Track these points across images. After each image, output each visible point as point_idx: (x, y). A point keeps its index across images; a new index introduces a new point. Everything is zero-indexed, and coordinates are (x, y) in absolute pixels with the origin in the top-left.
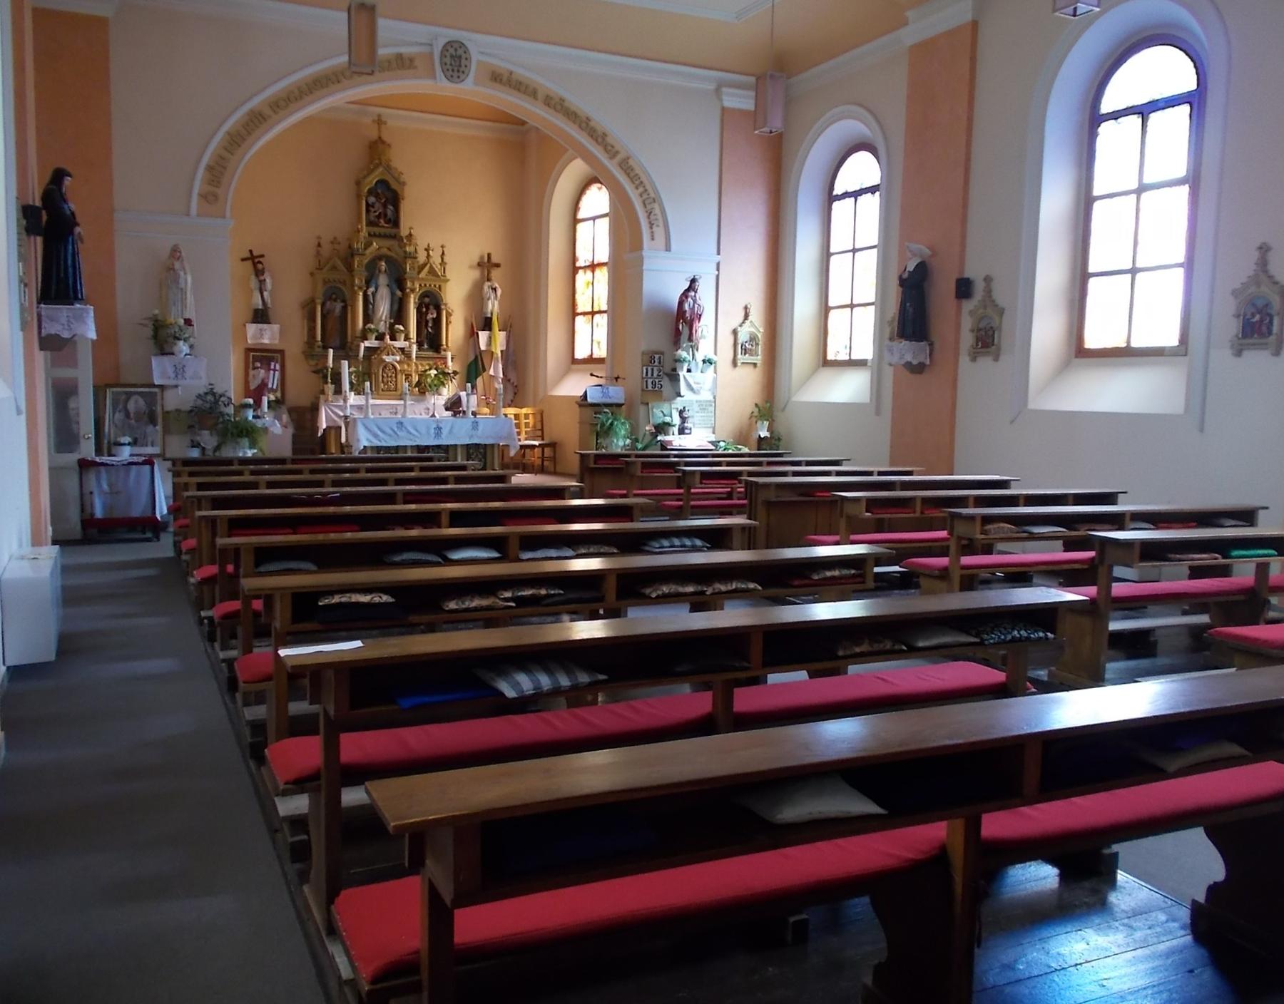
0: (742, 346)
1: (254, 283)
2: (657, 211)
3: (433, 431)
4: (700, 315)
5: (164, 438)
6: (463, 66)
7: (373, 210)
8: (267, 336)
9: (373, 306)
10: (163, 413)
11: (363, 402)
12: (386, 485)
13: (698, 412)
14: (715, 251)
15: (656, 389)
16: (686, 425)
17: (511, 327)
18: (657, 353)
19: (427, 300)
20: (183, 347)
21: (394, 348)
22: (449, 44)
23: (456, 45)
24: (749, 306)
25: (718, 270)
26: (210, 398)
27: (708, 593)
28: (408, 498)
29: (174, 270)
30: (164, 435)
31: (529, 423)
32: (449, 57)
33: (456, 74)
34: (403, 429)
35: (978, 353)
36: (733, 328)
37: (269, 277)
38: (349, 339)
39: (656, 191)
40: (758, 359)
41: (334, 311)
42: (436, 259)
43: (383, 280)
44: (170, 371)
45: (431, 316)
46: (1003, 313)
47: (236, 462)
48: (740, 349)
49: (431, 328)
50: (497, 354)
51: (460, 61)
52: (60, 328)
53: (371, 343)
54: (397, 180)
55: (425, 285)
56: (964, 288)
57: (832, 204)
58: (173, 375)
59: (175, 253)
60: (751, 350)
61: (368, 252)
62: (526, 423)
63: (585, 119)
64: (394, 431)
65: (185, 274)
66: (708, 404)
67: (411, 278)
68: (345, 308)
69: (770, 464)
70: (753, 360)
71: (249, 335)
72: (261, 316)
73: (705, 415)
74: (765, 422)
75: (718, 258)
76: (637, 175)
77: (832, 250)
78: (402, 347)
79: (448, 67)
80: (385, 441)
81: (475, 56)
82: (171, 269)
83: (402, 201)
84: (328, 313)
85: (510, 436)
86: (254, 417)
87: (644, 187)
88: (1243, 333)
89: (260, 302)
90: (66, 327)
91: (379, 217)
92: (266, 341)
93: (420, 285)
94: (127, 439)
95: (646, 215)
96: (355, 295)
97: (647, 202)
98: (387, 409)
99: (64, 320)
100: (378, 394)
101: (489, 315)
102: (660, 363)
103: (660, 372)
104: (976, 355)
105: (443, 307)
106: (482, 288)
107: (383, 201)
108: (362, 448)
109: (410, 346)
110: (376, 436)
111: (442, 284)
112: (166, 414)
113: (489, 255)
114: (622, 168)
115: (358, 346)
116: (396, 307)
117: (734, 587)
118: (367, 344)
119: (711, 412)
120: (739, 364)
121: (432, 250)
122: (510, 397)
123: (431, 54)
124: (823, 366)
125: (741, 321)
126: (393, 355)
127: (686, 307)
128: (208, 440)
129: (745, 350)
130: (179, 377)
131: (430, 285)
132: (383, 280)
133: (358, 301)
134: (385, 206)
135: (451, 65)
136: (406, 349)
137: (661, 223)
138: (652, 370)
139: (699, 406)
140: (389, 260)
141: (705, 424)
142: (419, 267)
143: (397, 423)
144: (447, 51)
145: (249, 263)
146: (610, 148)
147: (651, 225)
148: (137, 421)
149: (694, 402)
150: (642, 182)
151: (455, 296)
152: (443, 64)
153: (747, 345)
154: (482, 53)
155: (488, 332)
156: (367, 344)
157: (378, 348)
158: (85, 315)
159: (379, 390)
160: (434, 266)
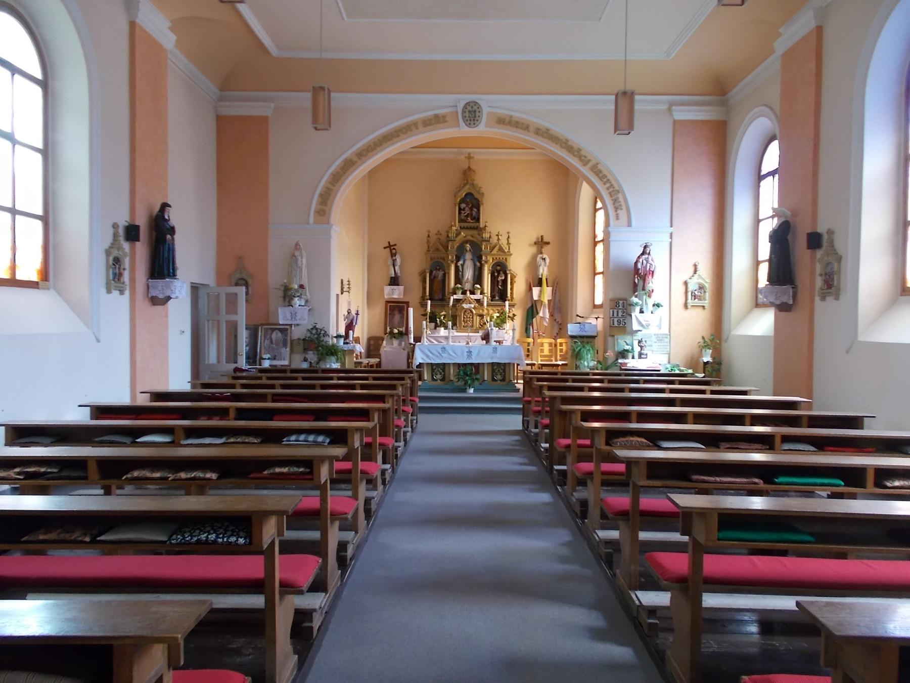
0: (692, 293)
1: (390, 262)
2: (621, 199)
3: (466, 354)
4: (653, 272)
5: (290, 356)
6: (477, 116)
7: (463, 212)
8: (397, 293)
9: (463, 272)
10: (291, 340)
11: (447, 335)
12: (314, 389)
13: (655, 342)
14: (669, 224)
15: (621, 325)
16: (642, 351)
17: (557, 284)
18: (621, 300)
19: (498, 268)
20: (297, 302)
21: (472, 299)
22: (468, 104)
23: (471, 104)
24: (697, 264)
25: (671, 238)
26: (314, 332)
27: (170, 479)
28: (275, 398)
29: (295, 256)
30: (291, 354)
31: (562, 349)
32: (467, 112)
33: (472, 122)
34: (446, 352)
35: (826, 293)
36: (685, 280)
37: (399, 257)
38: (446, 293)
39: (620, 186)
40: (707, 303)
41: (438, 277)
42: (503, 241)
43: (468, 256)
44: (289, 317)
45: (501, 278)
46: (841, 259)
47: (320, 371)
48: (692, 296)
49: (501, 286)
50: (545, 303)
51: (475, 114)
52: (158, 292)
53: (459, 296)
54: (478, 192)
55: (496, 258)
56: (815, 241)
57: (761, 181)
58: (290, 318)
59: (297, 246)
60: (700, 296)
61: (458, 239)
62: (560, 349)
63: (564, 140)
64: (439, 353)
65: (302, 258)
66: (664, 336)
67: (485, 254)
68: (444, 275)
69: (646, 382)
70: (702, 303)
71: (386, 293)
72: (394, 281)
73: (662, 344)
74: (708, 350)
75: (671, 230)
76: (605, 175)
77: (760, 218)
78: (479, 298)
79: (467, 118)
80: (433, 360)
81: (486, 110)
82: (294, 255)
83: (481, 205)
84: (435, 277)
85: (519, 358)
86: (344, 343)
87: (610, 183)
88: (400, 270)
89: (393, 273)
90: (161, 292)
91: (467, 216)
92: (395, 296)
93: (493, 258)
94: (268, 356)
95: (612, 202)
96: (449, 266)
97: (613, 194)
98: (465, 339)
99: (160, 288)
100: (460, 329)
101: (540, 277)
102: (623, 307)
103: (624, 313)
104: (824, 295)
105: (508, 272)
106: (537, 257)
107: (470, 206)
108: (418, 364)
109: (483, 298)
110: (427, 356)
111: (508, 257)
112: (292, 341)
113: (542, 236)
114: (593, 171)
115: (450, 298)
116: (477, 273)
117: (193, 476)
118: (455, 297)
119: (667, 342)
120: (689, 307)
121: (501, 236)
122: (556, 331)
123: (457, 112)
124: (756, 307)
125: (692, 275)
126: (470, 304)
127: (639, 266)
128: (312, 356)
129: (695, 296)
130: (293, 319)
131: (500, 258)
132: (468, 256)
133: (451, 270)
134: (471, 209)
135: (469, 117)
136: (481, 300)
137: (624, 207)
138: (618, 311)
139: (657, 338)
140: (472, 244)
141: (661, 351)
142: (492, 246)
143: (442, 348)
144: (466, 108)
145: (388, 249)
146: (583, 158)
147: (616, 209)
148: (276, 345)
149: (653, 335)
150: (608, 180)
151: (518, 265)
152: (464, 117)
153: (696, 292)
154: (490, 107)
155: (539, 288)
156: (455, 297)
157: (461, 299)
158: (171, 284)
159: (461, 326)
160: (502, 246)
